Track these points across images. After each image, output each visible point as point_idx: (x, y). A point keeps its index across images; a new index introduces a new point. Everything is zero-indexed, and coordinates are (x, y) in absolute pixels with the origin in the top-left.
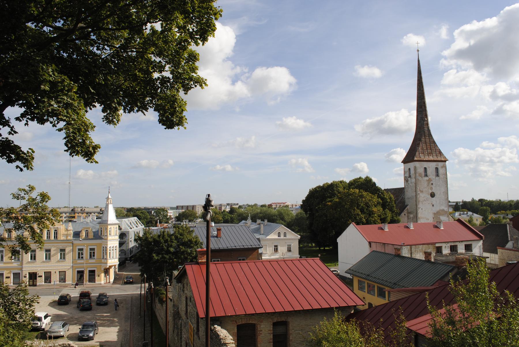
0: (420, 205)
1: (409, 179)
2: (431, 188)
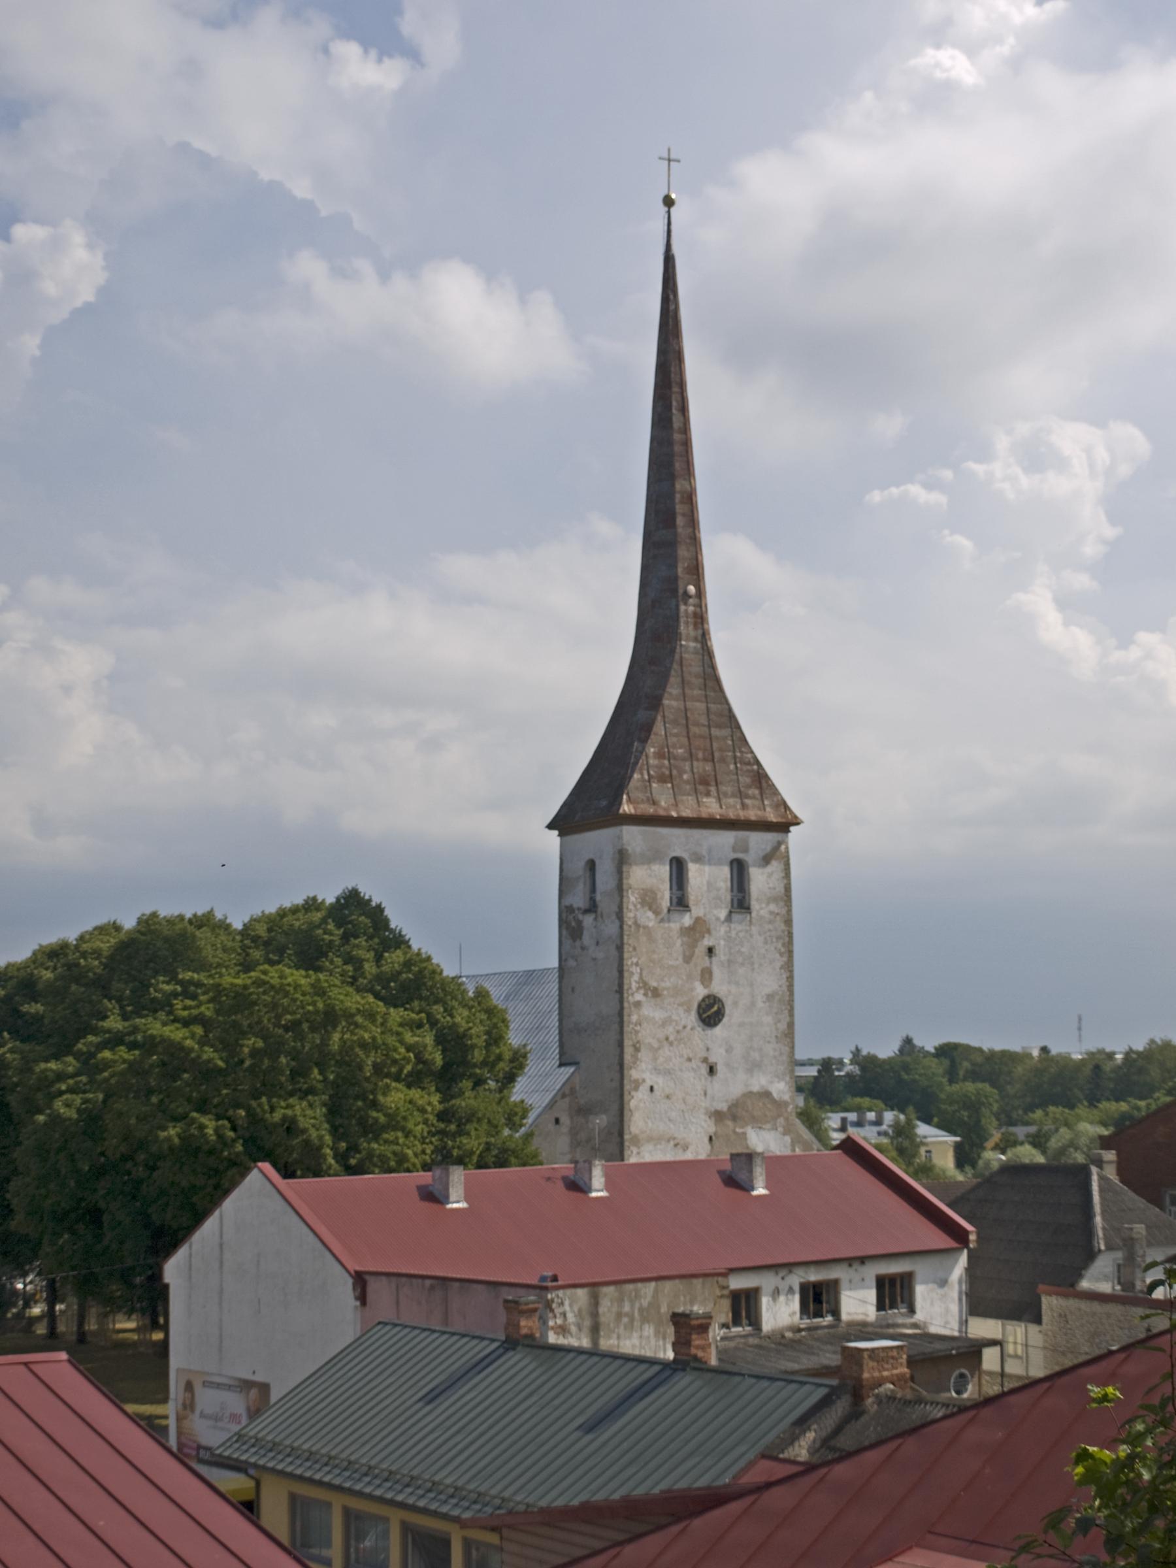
1: (588, 920)
2: (706, 976)
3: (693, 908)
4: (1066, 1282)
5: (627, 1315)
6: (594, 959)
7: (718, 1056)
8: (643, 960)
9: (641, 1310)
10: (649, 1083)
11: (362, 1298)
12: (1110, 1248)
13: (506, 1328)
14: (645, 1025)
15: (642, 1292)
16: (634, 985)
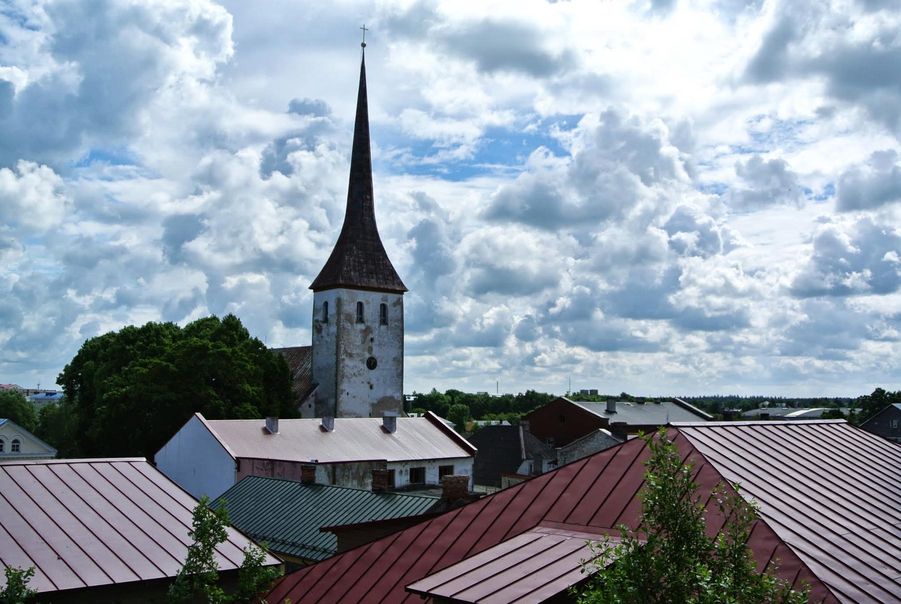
0: (345, 386)
1: (324, 326)
2: (370, 350)
3: (366, 323)
4: (513, 473)
5: (347, 476)
6: (327, 341)
7: (374, 382)
8: (345, 343)
9: (352, 474)
10: (347, 391)
11: (238, 469)
12: (528, 458)
13: (302, 478)
14: (346, 367)
15: (353, 466)
16: (342, 352)
